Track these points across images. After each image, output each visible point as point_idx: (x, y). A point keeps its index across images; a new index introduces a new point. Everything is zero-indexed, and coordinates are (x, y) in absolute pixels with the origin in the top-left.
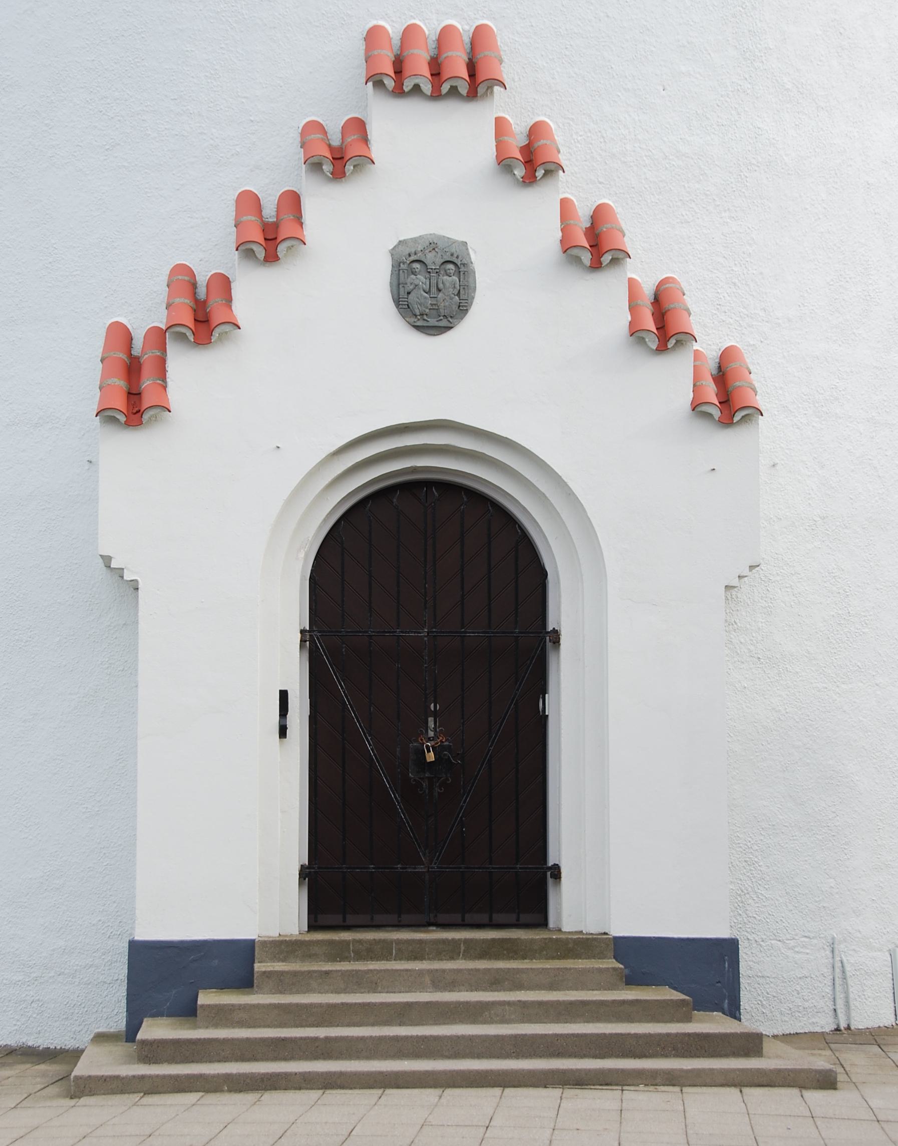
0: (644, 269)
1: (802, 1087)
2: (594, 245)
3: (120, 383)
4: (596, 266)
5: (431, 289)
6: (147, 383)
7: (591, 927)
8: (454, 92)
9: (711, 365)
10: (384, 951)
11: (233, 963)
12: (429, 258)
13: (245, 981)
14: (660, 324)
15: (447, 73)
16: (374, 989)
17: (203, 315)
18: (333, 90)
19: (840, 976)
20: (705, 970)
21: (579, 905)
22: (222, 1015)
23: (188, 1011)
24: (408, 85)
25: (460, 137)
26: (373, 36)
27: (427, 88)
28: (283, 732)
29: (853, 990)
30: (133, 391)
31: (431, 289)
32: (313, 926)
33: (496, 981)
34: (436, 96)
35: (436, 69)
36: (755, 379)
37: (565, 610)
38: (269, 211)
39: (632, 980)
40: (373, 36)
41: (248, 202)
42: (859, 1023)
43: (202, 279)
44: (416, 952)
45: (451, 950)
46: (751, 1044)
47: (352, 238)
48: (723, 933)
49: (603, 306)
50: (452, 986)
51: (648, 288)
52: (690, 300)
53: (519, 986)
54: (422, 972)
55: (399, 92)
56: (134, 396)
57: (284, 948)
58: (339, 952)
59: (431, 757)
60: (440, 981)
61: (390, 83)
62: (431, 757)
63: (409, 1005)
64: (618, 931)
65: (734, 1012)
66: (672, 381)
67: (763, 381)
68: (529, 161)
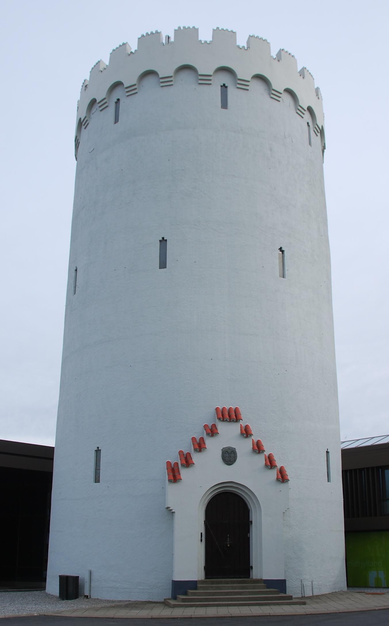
0: (255, 438)
1: (300, 605)
2: (258, 448)
3: (171, 474)
4: (259, 453)
5: (229, 456)
6: (176, 474)
7: (259, 578)
8: (233, 421)
9: (279, 469)
10: (221, 583)
11: (193, 585)
12: (229, 451)
13: (196, 588)
14: (270, 463)
15: (231, 416)
16: (221, 590)
17: (187, 461)
18: (207, 416)
19: (303, 586)
20: (280, 585)
21: (255, 574)
22: (194, 594)
23: (186, 594)
24: (225, 420)
25: (235, 429)
26: (217, 409)
27: (228, 420)
28: (201, 541)
29: (305, 589)
30: (174, 476)
31: (229, 456)
32: (206, 578)
33: (243, 588)
34: (230, 421)
35: (230, 416)
36: (287, 473)
37: (253, 517)
38: (198, 440)
39: (268, 587)
40: (217, 409)
41: (194, 439)
42: (306, 596)
43: (185, 453)
44: (227, 583)
45: (233, 582)
46: (290, 598)
47: (214, 447)
48: (283, 578)
49: (260, 460)
50: (235, 589)
51: (255, 441)
52: (263, 444)
53: (247, 589)
54: (228, 586)
55: (223, 421)
56: (174, 476)
57: (202, 582)
58: (213, 583)
59: (229, 545)
60: (233, 588)
61: (222, 419)
62: (229, 545)
63: (229, 592)
64: (264, 578)
65: (285, 593)
66: (273, 474)
67: (289, 473)
68: (246, 433)
